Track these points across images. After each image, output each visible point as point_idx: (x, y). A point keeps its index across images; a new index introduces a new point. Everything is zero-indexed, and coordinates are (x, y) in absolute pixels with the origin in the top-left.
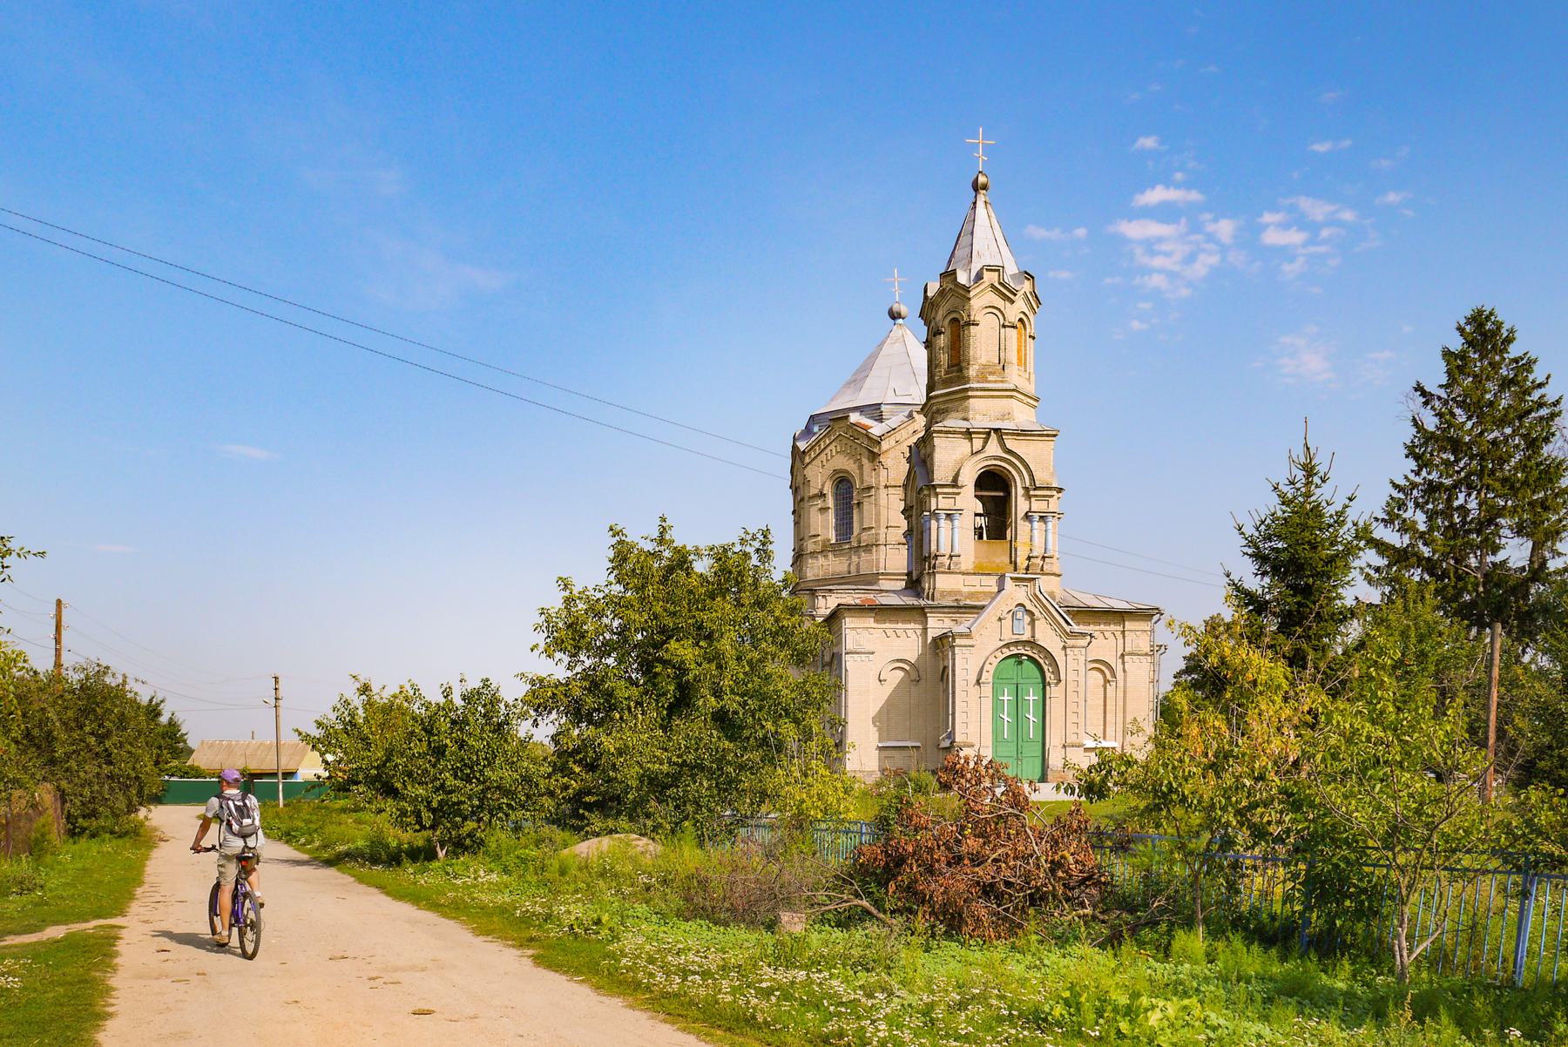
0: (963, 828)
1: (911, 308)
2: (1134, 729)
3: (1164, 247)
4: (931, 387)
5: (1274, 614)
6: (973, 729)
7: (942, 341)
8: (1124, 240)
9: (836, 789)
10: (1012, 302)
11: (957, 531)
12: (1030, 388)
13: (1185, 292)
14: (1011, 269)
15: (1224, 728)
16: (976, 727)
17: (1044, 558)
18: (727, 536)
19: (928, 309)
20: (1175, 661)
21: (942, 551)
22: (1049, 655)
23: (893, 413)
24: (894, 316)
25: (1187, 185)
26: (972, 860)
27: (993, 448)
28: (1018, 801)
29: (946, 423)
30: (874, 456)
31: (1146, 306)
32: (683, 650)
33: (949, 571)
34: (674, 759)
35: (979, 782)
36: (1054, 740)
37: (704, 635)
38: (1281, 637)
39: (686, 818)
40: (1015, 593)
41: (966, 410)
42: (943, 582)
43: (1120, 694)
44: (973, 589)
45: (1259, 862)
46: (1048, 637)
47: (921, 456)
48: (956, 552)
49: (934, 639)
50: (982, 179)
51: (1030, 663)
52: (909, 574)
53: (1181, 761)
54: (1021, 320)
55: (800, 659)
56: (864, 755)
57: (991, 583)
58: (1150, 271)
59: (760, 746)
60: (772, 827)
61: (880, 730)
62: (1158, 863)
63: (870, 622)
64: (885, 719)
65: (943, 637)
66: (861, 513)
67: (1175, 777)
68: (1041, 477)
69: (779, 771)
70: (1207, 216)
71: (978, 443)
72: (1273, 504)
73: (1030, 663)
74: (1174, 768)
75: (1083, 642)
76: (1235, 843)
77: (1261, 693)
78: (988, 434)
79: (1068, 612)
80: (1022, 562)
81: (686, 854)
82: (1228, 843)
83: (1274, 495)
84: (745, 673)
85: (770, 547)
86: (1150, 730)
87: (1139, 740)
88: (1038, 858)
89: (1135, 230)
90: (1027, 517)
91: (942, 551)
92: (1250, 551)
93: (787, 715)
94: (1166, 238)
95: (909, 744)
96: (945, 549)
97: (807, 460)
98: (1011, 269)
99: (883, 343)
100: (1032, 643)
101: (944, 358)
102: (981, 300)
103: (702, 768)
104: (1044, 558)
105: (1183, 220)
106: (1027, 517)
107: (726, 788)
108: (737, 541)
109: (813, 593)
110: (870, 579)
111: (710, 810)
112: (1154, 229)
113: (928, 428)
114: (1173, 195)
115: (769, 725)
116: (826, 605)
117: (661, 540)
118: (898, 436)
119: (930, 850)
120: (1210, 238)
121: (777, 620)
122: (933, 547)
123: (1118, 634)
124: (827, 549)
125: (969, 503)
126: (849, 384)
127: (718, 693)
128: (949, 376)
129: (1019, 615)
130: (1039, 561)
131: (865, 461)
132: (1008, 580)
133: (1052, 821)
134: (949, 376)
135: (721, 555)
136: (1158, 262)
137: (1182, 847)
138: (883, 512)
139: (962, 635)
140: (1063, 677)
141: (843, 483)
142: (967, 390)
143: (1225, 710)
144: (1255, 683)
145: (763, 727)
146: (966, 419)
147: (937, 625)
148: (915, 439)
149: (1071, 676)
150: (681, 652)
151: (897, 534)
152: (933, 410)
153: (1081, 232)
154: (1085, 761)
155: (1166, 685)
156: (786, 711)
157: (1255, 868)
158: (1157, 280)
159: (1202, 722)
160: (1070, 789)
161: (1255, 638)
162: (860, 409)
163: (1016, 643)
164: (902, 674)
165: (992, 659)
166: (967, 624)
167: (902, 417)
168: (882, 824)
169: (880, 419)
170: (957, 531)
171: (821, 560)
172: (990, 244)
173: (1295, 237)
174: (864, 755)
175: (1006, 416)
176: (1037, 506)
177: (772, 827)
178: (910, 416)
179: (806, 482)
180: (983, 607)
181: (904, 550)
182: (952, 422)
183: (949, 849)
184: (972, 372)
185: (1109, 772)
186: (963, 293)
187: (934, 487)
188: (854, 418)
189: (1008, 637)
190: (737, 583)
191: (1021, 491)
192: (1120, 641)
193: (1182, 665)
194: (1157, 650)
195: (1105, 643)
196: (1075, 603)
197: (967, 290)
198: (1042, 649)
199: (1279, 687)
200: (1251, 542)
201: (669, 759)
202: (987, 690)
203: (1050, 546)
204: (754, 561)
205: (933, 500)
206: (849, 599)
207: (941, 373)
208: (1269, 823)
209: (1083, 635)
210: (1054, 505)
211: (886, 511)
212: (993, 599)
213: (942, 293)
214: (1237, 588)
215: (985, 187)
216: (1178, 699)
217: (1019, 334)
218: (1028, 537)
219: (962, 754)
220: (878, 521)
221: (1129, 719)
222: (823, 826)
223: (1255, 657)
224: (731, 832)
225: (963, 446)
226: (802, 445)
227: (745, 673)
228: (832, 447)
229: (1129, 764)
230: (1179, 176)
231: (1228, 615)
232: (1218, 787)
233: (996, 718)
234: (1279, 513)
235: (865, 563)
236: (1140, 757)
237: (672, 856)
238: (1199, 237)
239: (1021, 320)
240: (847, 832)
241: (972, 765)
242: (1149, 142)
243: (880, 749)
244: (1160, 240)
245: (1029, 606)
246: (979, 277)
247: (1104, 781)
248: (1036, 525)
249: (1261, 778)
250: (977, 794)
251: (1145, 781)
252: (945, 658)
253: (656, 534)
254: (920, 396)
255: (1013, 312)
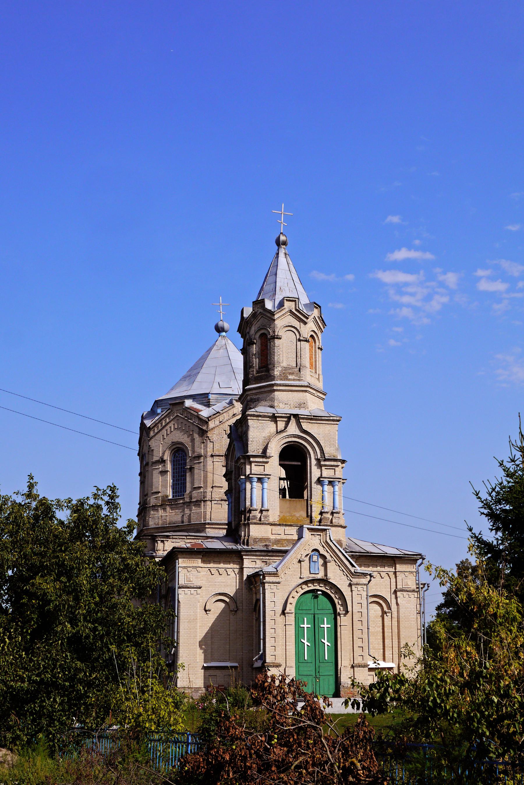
0: (271, 738)
1: (232, 324)
2: (404, 652)
3: (410, 290)
4: (246, 382)
5: (506, 561)
6: (280, 652)
7: (254, 349)
8: (381, 284)
9: (168, 703)
10: (305, 323)
11: (266, 492)
12: (320, 385)
13: (426, 321)
14: (304, 300)
15: (474, 652)
16: (282, 650)
17: (332, 513)
18: (81, 491)
19: (244, 327)
20: (436, 596)
21: (255, 507)
22: (338, 591)
23: (218, 401)
24: (219, 330)
25: (423, 249)
26: (278, 767)
27: (293, 429)
28: (314, 713)
29: (257, 409)
30: (203, 433)
31: (399, 329)
32: (47, 585)
33: (260, 522)
34: (34, 678)
35: (283, 698)
36: (344, 662)
37: (65, 571)
38: (514, 579)
39: (40, 731)
40: (310, 541)
41: (273, 400)
42: (256, 531)
43: (395, 623)
44: (279, 537)
45: (509, 767)
46: (337, 576)
47: (239, 433)
48: (266, 507)
49: (248, 577)
50: (282, 238)
51: (323, 597)
52: (229, 524)
53: (442, 680)
54: (312, 336)
55: (140, 592)
56: (191, 674)
57: (293, 532)
58: (401, 306)
59: (106, 666)
60: (113, 738)
61: (205, 652)
62: (429, 768)
63: (198, 562)
64: (208, 643)
65: (256, 575)
66: (192, 475)
67: (439, 694)
68: (329, 451)
69: (121, 688)
70: (438, 270)
71: (281, 425)
72: (501, 474)
73: (323, 597)
74: (438, 686)
75: (365, 581)
76: (489, 752)
77: (501, 624)
78: (289, 418)
79: (352, 557)
80: (316, 516)
81: (38, 764)
82: (483, 750)
83: (501, 469)
84: (96, 604)
85: (117, 500)
86: (419, 653)
87: (411, 662)
88: (332, 765)
89: (387, 277)
90: (319, 481)
91: (255, 507)
92: (486, 511)
93: (129, 640)
94: (408, 282)
95: (228, 664)
96: (257, 505)
97: (152, 434)
98: (304, 300)
99: (210, 349)
100: (325, 581)
101: (256, 362)
102: (282, 322)
103: (54, 685)
104: (261, 511)
105: (422, 272)
106: (319, 481)
107: (75, 704)
108: (90, 496)
109: (154, 540)
110: (200, 528)
111: (62, 723)
112: (402, 277)
113: (244, 412)
114: (413, 254)
115: (113, 648)
116: (164, 548)
117: (29, 495)
118: (221, 418)
119: (244, 759)
120: (442, 284)
121: (124, 559)
122: (248, 503)
123: (391, 574)
124: (165, 503)
125: (275, 470)
126: (185, 378)
127: (73, 621)
128: (260, 375)
129: (315, 558)
130: (329, 516)
131: (196, 436)
132: (305, 531)
133: (342, 731)
134: (260, 375)
135: (78, 508)
136: (406, 299)
137: (448, 756)
138: (210, 475)
139: (270, 574)
140: (350, 609)
141: (179, 452)
142: (273, 385)
143: (474, 638)
144: (495, 615)
145: (109, 649)
146: (272, 407)
147: (251, 565)
148: (234, 420)
149: (356, 608)
150: (44, 586)
151: (220, 493)
152: (248, 399)
153: (350, 277)
154: (367, 679)
155: (431, 615)
156: (127, 636)
157: (505, 772)
158: (406, 312)
159: (458, 647)
160: (355, 704)
161: (493, 579)
162: (193, 397)
163: (313, 581)
164: (222, 605)
165: (294, 594)
166: (275, 565)
167: (224, 403)
168: (204, 735)
169: (208, 405)
170: (266, 492)
171: (161, 512)
172: (288, 282)
173: (500, 286)
174: (191, 674)
175: (301, 405)
176: (327, 473)
177: (113, 738)
178: (231, 403)
179: (151, 451)
180: (286, 552)
181: (225, 506)
182: (262, 409)
183: (259, 756)
184: (277, 372)
185: (386, 690)
186: (270, 316)
187: (249, 457)
188: (188, 403)
189: (307, 576)
190: (92, 531)
191: (314, 462)
192: (393, 580)
193: (441, 600)
194: (422, 587)
195: (381, 581)
196: (358, 549)
197: (272, 313)
198: (333, 586)
199: (514, 619)
200: (487, 505)
201: (29, 678)
202: (291, 619)
203: (337, 504)
204: (105, 511)
205: (248, 467)
206: (182, 544)
207: (254, 371)
208: (514, 733)
209: (364, 575)
210: (339, 473)
211: (214, 474)
212: (294, 545)
213: (254, 315)
214: (479, 540)
215: (285, 243)
216: (438, 628)
217: (311, 346)
218: (321, 498)
219: (269, 674)
220: (205, 482)
221: (402, 644)
222: (156, 737)
223: (494, 594)
224: (78, 743)
225: (271, 427)
226: (148, 423)
227: (96, 604)
228: (171, 425)
229: (402, 682)
230: (417, 242)
231: (474, 561)
232: (472, 702)
233: (299, 644)
234: (505, 483)
235: (195, 514)
236: (411, 676)
237: (26, 764)
238: (434, 284)
239: (312, 336)
240: (176, 742)
241: (277, 683)
242: (395, 219)
243: (204, 668)
244: (406, 284)
245: (322, 552)
246: (281, 305)
247: (383, 697)
248: (326, 488)
249: (506, 695)
250: (283, 709)
251: (415, 697)
252: (257, 592)
253: (26, 490)
254: (237, 388)
255: (306, 330)
